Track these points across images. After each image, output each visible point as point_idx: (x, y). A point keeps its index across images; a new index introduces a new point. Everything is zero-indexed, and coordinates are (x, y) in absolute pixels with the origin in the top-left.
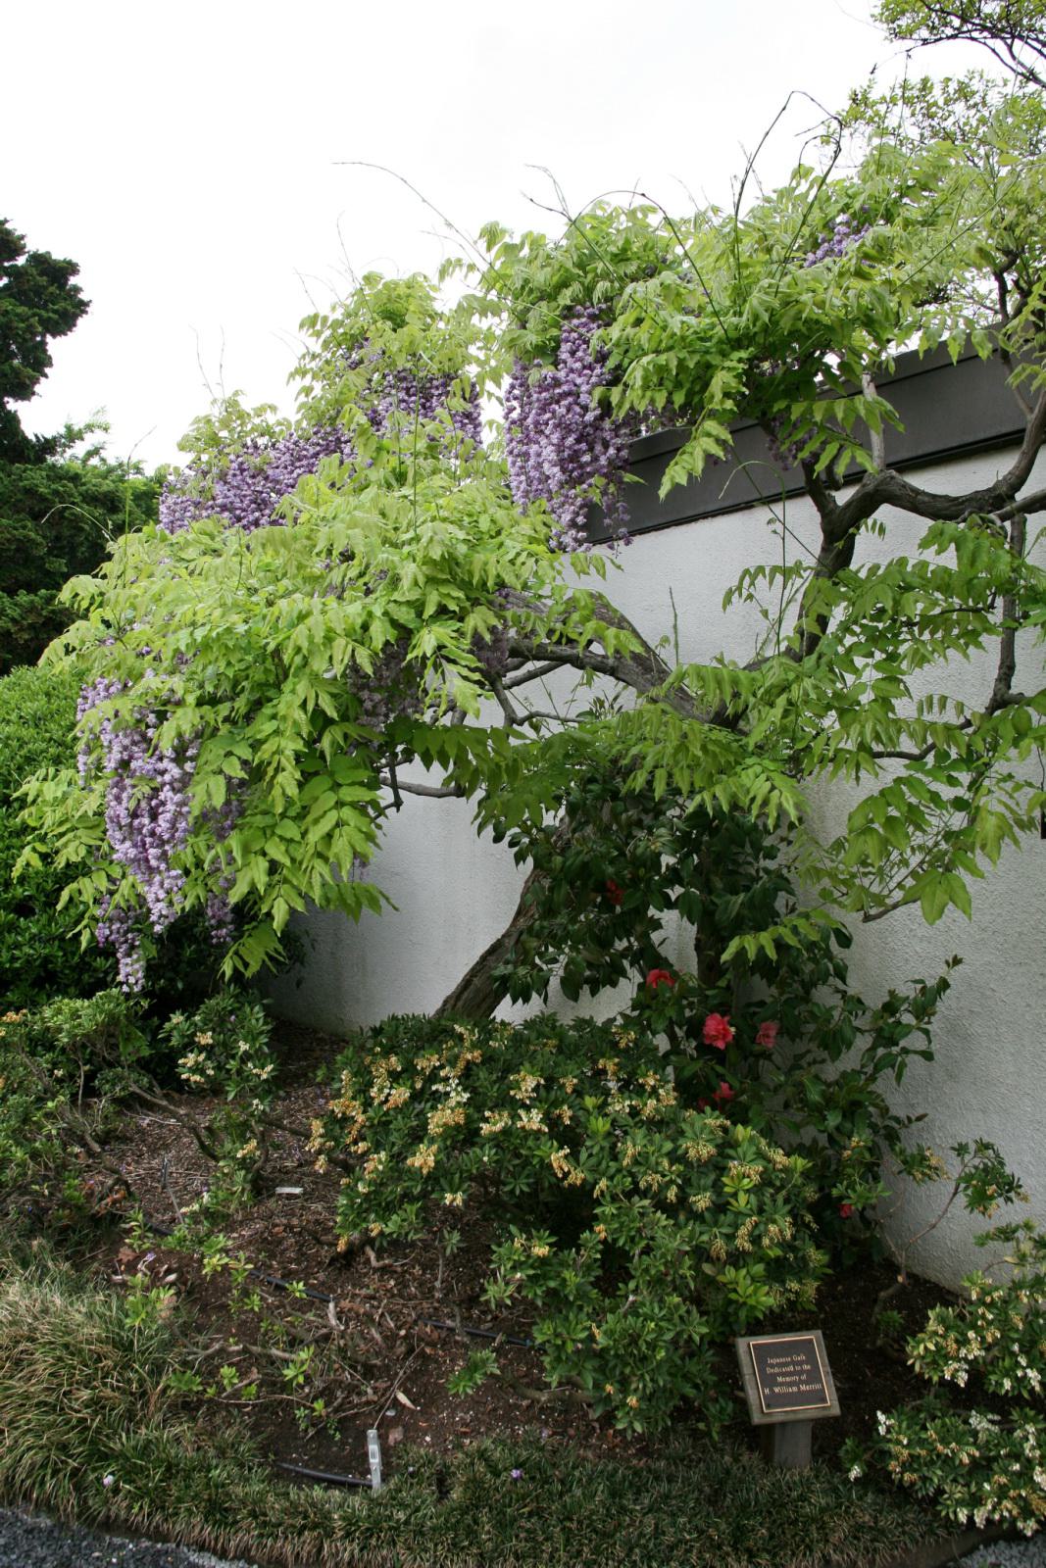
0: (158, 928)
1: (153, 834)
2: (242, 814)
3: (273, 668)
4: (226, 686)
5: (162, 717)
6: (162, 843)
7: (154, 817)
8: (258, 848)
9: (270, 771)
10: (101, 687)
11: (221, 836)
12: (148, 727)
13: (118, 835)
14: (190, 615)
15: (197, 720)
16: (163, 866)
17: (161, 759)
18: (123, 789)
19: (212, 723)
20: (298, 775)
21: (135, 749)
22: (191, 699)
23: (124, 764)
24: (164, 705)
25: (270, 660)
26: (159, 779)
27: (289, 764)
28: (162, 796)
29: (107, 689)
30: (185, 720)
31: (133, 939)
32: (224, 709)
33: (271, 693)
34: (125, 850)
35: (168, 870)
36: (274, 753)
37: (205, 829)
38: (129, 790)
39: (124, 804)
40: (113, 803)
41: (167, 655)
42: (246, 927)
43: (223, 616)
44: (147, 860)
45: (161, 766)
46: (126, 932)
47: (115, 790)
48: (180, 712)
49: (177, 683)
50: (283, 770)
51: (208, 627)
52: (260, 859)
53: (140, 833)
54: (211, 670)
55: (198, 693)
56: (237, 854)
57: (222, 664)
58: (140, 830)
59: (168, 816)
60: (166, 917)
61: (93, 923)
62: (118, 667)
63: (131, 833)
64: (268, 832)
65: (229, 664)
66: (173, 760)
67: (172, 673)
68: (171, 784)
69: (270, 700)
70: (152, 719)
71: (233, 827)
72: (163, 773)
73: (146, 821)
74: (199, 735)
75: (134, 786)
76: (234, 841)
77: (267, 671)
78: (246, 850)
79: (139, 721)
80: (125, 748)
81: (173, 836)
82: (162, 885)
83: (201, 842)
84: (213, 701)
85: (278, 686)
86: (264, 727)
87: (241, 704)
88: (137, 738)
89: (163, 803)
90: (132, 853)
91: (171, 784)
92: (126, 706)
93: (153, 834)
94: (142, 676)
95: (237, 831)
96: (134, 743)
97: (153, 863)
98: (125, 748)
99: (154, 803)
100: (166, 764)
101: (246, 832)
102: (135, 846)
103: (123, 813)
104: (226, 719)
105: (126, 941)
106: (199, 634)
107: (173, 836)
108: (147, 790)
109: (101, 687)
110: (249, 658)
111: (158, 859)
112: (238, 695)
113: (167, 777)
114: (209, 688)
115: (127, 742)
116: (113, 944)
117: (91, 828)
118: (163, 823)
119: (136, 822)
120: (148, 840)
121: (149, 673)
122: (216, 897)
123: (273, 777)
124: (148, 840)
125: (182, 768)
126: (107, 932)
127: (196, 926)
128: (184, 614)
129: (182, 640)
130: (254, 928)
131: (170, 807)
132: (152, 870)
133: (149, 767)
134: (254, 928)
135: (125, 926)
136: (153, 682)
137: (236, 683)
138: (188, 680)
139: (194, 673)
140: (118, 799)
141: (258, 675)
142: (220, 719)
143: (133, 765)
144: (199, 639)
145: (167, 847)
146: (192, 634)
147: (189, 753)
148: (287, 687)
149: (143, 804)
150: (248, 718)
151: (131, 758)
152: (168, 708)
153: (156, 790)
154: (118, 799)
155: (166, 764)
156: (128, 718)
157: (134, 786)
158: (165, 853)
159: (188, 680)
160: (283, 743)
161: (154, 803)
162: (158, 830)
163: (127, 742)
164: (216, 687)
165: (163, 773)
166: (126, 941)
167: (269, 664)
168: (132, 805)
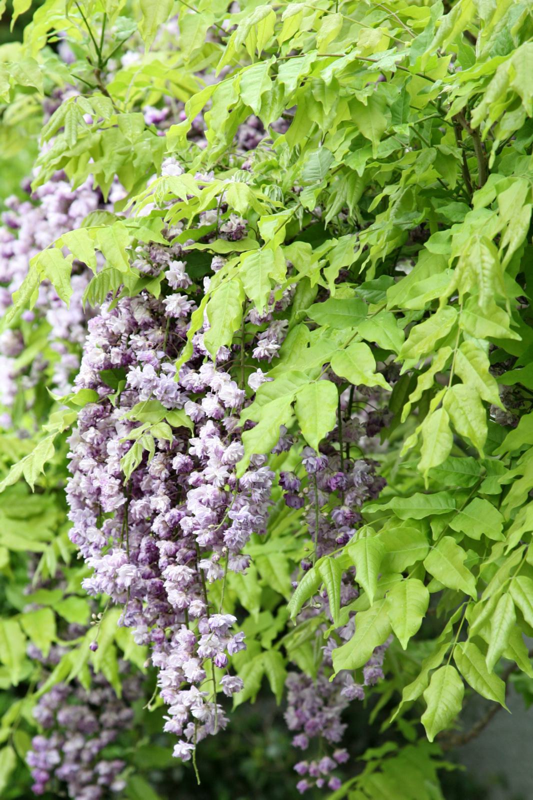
0: (181, 749)
1: (174, 533)
2: (373, 492)
3: (458, 153)
4: (346, 195)
5: (199, 265)
6: (196, 555)
7: (177, 496)
8: (410, 562)
9: (425, 382)
10: (50, 203)
11: (329, 540)
12: (167, 290)
13: (95, 535)
14: (266, 29)
15: (280, 275)
16: (196, 606)
17: (196, 364)
18: (109, 432)
19: (316, 280)
20: (493, 393)
21: (137, 340)
22: (271, 228)
23: (113, 375)
24: (205, 240)
25: (451, 133)
26: (191, 408)
27: (473, 365)
28: (197, 447)
29: (66, 205)
30: (245, 281)
31: (111, 776)
32: (344, 252)
33: (449, 209)
34: (110, 567)
35: (208, 611)
36: (441, 343)
37: (283, 526)
38: (124, 434)
39: (113, 465)
40: (87, 463)
41: (216, 124)
42: (370, 753)
43: (343, 33)
44: (160, 594)
45: (194, 379)
46: (94, 761)
47: (92, 433)
48: (249, 258)
49: (236, 190)
50: (457, 380)
51: (311, 57)
52: (414, 584)
53: (146, 531)
54: (315, 165)
55: (287, 213)
56: (365, 577)
57: (340, 146)
58: (144, 526)
59: (209, 492)
60: (199, 723)
61: (21, 737)
62: (98, 151)
63: (124, 533)
64: (436, 529)
65: (360, 143)
66: (223, 366)
67: (221, 168)
68: (217, 420)
69: (444, 226)
70: (176, 272)
71: (356, 521)
72: (198, 395)
73: (160, 501)
74: (282, 310)
75: (133, 424)
76: (360, 551)
77: (443, 160)
78: (385, 569)
79: (147, 278)
80: (115, 339)
81: (219, 538)
82: (193, 646)
83: (274, 554)
84: (313, 231)
85: (465, 196)
86: (423, 284)
87: (379, 239)
88: (142, 315)
89: (198, 464)
90: (128, 575)
91: (217, 420)
92: (112, 244)
93: (174, 533)
94: (152, 170)
95: (366, 529)
96: (135, 327)
97: (175, 598)
98: (115, 339)
99: (178, 461)
100: (208, 374)
101: (389, 528)
102: (133, 559)
103: (110, 486)
104: (345, 276)
105: (93, 781)
106: (291, 73)
107: (219, 538)
108: (164, 433)
109: (50, 203)
110: (404, 131)
111: (187, 588)
112: (369, 218)
113: (209, 405)
114: (309, 201)
115: (119, 325)
116: (64, 785)
117: (28, 518)
118: (198, 506)
119: (137, 506)
120: (165, 546)
121: (170, 167)
122: (307, 683)
123: (429, 395)
124: (165, 546)
125: (243, 385)
126: (54, 758)
127: (247, 755)
128: (253, 28)
129: (252, 86)
130: (388, 755)
131: (214, 471)
132: (170, 616)
133: (167, 381)
134: (388, 755)
135: (93, 746)
136: (181, 184)
137: (369, 189)
138: (258, 185)
139: (271, 168)
140: (98, 454)
141: (422, 171)
142: (332, 274)
143: (134, 376)
144: (291, 86)
145: (204, 564)
146: (274, 70)
147: (258, 352)
148: (480, 198)
149: (155, 465)
150: (389, 268)
151: (128, 360)
152: (216, 246)
153: (183, 434)
154: (98, 454)
155: (208, 374)
156: (123, 267)
157: (133, 424)
158: (199, 579)
159: (258, 185)
160: (465, 323)
161: (178, 461)
162: (186, 524)
163: (119, 325)
164: (322, 202)
165: (198, 395)
166: (93, 781)
167: (448, 144)
168: (129, 464)
